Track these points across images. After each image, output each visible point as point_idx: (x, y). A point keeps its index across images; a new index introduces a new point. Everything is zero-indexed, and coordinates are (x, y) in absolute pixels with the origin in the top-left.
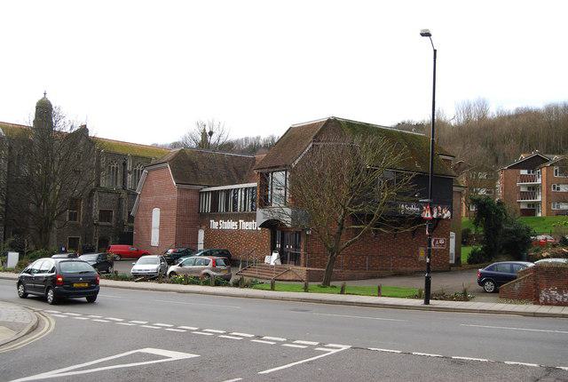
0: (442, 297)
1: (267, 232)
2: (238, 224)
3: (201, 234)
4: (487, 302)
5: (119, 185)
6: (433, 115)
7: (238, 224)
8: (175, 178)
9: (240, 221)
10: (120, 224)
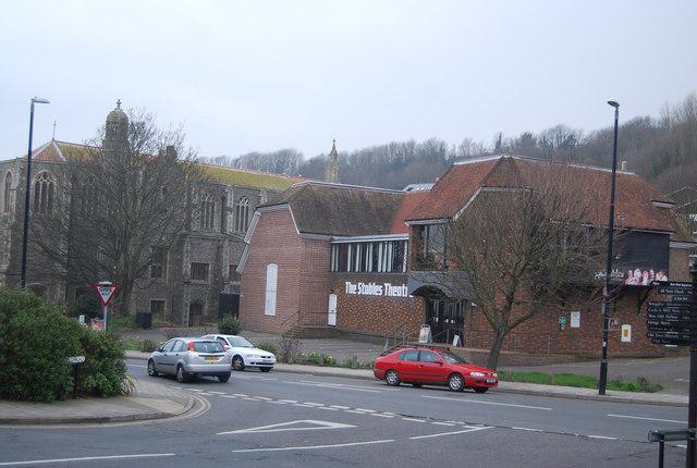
0: (618, 385)
1: (421, 300)
2: (384, 288)
3: (333, 301)
4: (674, 394)
5: (217, 229)
6: (617, 121)
7: (384, 288)
8: (299, 224)
9: (386, 285)
10: (219, 282)
